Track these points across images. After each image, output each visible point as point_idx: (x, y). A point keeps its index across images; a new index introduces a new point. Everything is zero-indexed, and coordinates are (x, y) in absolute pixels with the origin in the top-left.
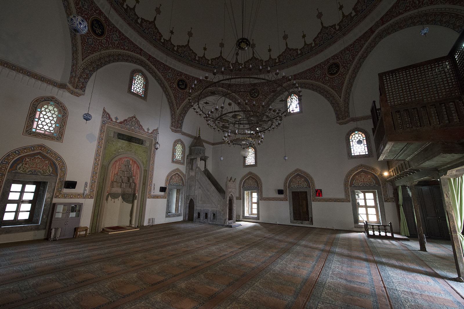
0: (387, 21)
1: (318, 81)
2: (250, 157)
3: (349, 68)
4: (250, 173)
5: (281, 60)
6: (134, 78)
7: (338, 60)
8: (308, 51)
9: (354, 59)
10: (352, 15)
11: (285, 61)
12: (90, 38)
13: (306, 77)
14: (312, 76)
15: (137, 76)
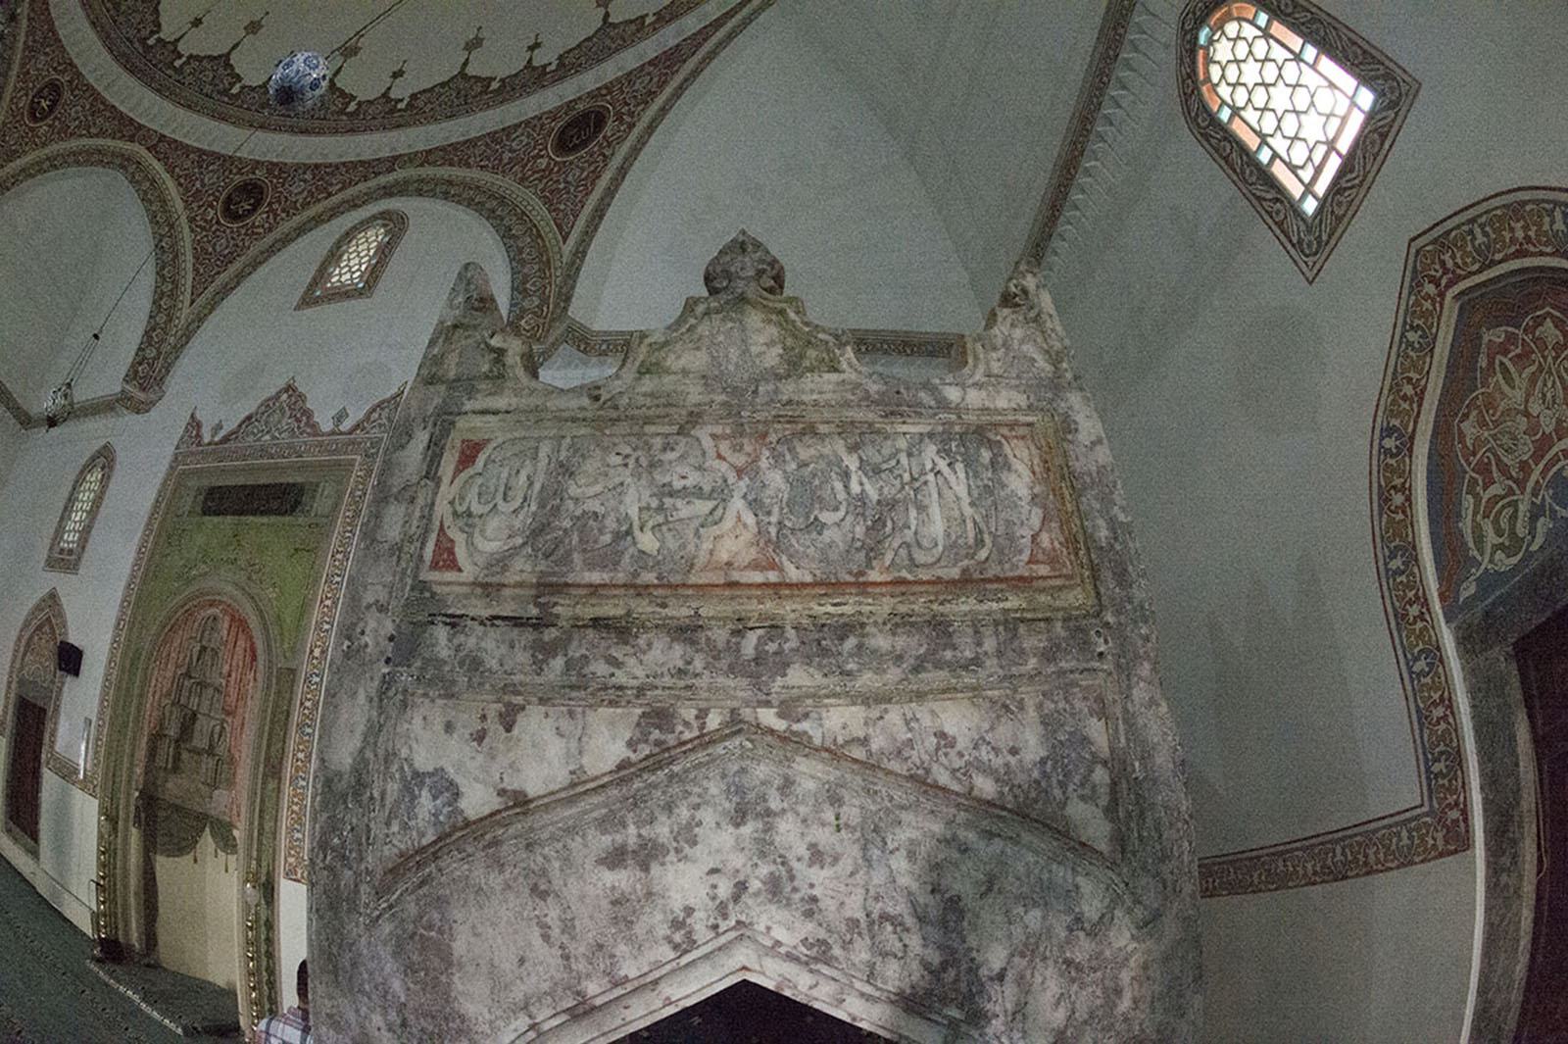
0: (434, 164)
2: (1280, 98)
5: (187, 70)
9: (306, 205)
11: (190, 79)
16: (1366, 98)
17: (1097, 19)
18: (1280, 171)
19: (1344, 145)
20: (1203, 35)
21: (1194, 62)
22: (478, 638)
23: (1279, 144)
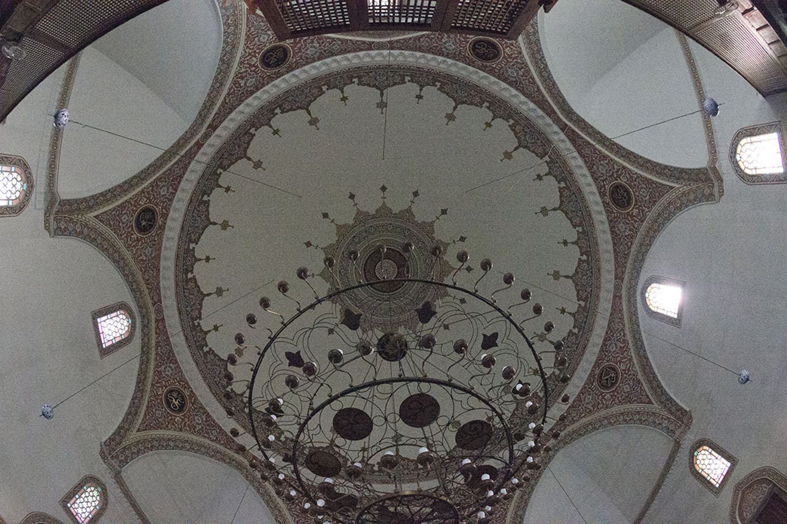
1: (636, 232)
2: (713, 467)
3: (619, 166)
4: (738, 487)
6: (85, 488)
7: (606, 186)
8: (586, 242)
10: (488, 105)
12: (128, 217)
13: (624, 254)
14: (626, 242)
15: (92, 489)
16: (729, 464)
17: (11, 99)
18: (712, 481)
19: (724, 474)
20: (696, 453)
21: (693, 459)
22: (340, 457)
23: (712, 476)
